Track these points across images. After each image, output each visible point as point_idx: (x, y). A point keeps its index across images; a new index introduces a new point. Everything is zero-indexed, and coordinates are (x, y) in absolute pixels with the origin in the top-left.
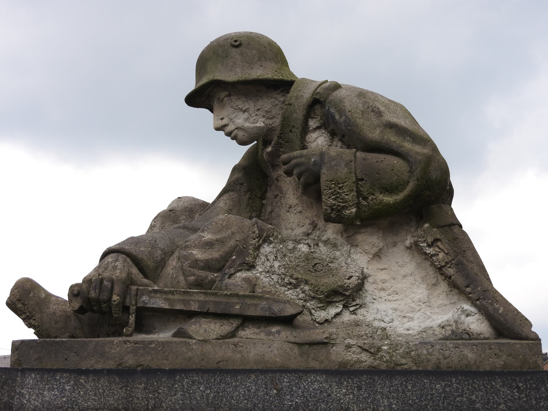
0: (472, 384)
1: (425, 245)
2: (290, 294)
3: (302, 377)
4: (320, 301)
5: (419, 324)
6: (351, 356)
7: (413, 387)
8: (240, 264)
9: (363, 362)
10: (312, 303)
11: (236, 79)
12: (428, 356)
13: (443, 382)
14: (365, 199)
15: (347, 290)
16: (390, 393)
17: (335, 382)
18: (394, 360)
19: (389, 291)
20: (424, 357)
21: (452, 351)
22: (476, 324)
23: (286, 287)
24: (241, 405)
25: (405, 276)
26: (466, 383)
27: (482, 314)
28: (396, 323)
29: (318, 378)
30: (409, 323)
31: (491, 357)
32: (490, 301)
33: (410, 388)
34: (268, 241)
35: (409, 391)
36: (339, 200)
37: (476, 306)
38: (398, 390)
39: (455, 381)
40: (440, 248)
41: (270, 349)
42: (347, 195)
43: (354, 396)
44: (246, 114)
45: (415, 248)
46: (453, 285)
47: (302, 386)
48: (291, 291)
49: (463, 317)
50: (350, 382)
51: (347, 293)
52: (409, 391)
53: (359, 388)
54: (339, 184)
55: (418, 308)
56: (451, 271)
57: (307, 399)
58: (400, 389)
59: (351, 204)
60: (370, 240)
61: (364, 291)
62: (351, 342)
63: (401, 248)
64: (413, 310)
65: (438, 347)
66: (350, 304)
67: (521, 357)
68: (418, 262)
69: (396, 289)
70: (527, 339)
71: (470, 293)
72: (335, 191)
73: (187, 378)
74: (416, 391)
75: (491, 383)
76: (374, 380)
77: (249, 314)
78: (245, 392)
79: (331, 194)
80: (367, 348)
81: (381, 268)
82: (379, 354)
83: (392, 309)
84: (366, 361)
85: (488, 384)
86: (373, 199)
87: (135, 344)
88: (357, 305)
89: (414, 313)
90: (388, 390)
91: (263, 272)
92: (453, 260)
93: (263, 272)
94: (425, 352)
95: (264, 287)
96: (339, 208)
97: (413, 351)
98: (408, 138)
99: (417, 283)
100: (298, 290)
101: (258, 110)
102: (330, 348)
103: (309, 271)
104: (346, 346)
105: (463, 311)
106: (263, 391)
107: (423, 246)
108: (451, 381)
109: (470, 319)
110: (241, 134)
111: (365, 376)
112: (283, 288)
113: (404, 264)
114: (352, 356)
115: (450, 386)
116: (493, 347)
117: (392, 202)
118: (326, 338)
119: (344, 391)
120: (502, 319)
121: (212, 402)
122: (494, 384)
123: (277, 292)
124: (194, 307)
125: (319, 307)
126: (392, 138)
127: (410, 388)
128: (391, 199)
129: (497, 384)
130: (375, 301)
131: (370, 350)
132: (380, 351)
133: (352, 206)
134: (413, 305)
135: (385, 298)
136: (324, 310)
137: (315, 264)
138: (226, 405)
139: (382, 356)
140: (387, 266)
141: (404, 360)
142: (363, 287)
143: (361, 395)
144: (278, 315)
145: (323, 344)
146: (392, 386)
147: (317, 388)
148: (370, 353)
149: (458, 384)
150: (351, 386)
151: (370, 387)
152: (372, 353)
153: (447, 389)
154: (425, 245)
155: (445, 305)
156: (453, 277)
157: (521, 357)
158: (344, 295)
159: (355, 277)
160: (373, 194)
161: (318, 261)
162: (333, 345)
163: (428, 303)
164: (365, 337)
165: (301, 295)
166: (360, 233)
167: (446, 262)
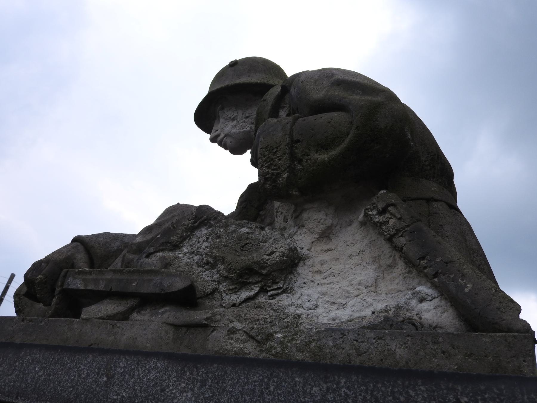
0: (372, 391)
1: (375, 212)
2: (206, 275)
3: (141, 361)
4: (232, 281)
5: (351, 313)
6: (232, 344)
7: (277, 387)
8: (163, 243)
9: (246, 353)
10: (225, 284)
11: (240, 100)
12: (334, 350)
13: (326, 383)
14: (300, 161)
15: (264, 268)
16: (242, 394)
17: (177, 371)
18: (286, 354)
19: (326, 274)
20: (328, 351)
21: (372, 344)
22: (432, 311)
23: (203, 267)
24: (64, 394)
25: (351, 256)
26: (362, 388)
27: (446, 299)
28: (320, 310)
29: (159, 364)
30: (337, 312)
31: (435, 357)
32: (452, 276)
33: (272, 388)
34: (208, 224)
35: (270, 393)
36: (273, 167)
37: (435, 286)
38: (254, 391)
39: (345, 383)
40: (391, 214)
41: (144, 332)
42: (280, 160)
43: (193, 394)
44: (235, 122)
45: (367, 223)
46: (409, 263)
47: (136, 374)
48: (207, 272)
49: (414, 302)
50: (195, 373)
51: (264, 272)
52: (270, 393)
53: (203, 383)
54: (273, 149)
55: (356, 293)
56: (401, 241)
57: (135, 393)
58: (257, 390)
59: (283, 169)
60: (317, 218)
61: (296, 275)
62: (237, 325)
63: (355, 224)
64: (348, 297)
65: (351, 336)
66: (270, 287)
67: (490, 358)
68: (373, 239)
69: (333, 271)
70: (509, 330)
71: (425, 268)
72: (269, 157)
73: (30, 355)
74: (279, 394)
75: (407, 393)
76: (226, 372)
77: (142, 291)
78: (75, 377)
79: (265, 161)
80: (253, 334)
81: (326, 249)
82: (268, 344)
83: (319, 293)
84: (250, 353)
85: (401, 394)
86: (307, 160)
87: (30, 322)
88: (278, 288)
89: (348, 299)
90: (240, 389)
91: (188, 253)
92: (408, 226)
93: (188, 253)
94: (331, 343)
95: (179, 267)
96: (274, 177)
97: (314, 340)
98: (358, 91)
99: (364, 264)
100: (215, 270)
101: (247, 117)
102: (209, 332)
103: (235, 250)
104: (228, 331)
105: (415, 294)
106: (93, 377)
107: (373, 215)
108: (338, 383)
109: (425, 305)
110: (228, 140)
111: (215, 365)
112: (201, 269)
113: (354, 242)
114: (233, 346)
115: (334, 390)
116: (441, 339)
117: (326, 159)
118: (207, 319)
119: (183, 385)
120: (469, 301)
121: (39, 387)
122: (412, 393)
123: (190, 272)
124: (101, 287)
125: (229, 290)
126: (338, 93)
127: (272, 388)
128: (326, 156)
129: (417, 394)
130: (305, 285)
131: (256, 337)
132: (270, 340)
133: (284, 171)
134: (350, 289)
135: (318, 282)
136: (236, 293)
137: (246, 244)
138: (50, 392)
139: (271, 347)
140: (333, 247)
141: (301, 354)
142: (296, 270)
143: (203, 393)
144: (166, 291)
145: (203, 326)
146: (247, 384)
147: (152, 378)
148: (257, 341)
149: (348, 388)
150: (194, 378)
151: (217, 382)
152: (259, 342)
153: (330, 396)
154: (375, 212)
155: (398, 291)
156: (404, 248)
157: (490, 358)
158: (261, 274)
159: (277, 253)
160: (308, 155)
161: (249, 241)
162: (214, 329)
163: (374, 287)
164: (261, 322)
165: (216, 276)
166: (306, 210)
167: (397, 230)
